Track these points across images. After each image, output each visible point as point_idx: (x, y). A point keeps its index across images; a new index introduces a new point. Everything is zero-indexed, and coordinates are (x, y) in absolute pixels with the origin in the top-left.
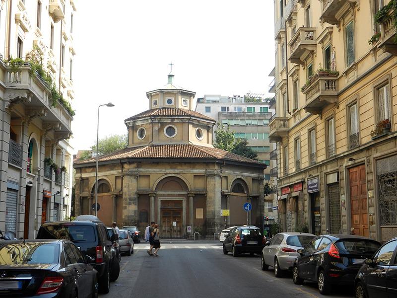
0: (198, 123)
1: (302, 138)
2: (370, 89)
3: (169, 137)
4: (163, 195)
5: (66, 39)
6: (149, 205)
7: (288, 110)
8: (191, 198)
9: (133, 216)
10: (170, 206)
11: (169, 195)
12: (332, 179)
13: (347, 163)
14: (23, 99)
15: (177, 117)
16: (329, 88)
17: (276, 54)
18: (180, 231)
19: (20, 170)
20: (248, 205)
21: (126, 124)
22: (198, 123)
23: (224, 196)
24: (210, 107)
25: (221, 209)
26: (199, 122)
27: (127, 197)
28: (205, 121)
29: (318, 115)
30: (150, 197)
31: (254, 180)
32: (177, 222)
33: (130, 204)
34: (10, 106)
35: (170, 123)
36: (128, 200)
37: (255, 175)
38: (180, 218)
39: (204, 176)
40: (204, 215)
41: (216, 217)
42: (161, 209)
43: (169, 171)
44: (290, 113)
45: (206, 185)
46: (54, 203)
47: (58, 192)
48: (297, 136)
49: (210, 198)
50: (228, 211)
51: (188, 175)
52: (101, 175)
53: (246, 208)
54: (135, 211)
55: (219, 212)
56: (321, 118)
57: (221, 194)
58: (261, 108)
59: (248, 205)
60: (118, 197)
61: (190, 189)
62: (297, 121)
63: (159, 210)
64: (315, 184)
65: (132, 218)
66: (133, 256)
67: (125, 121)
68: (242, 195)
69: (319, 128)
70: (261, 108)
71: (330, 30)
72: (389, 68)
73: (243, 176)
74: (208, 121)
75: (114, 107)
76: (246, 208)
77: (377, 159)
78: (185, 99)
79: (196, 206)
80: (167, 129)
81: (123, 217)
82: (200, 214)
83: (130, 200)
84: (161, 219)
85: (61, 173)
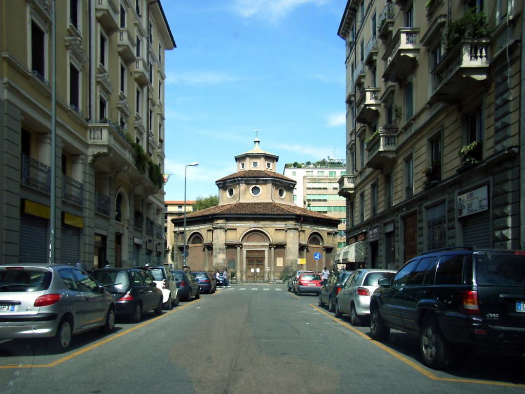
0: (280, 184)
1: (366, 193)
2: (424, 141)
3: (254, 195)
4: (249, 246)
5: (154, 105)
6: (236, 254)
7: (355, 169)
8: (273, 249)
9: (222, 264)
10: (255, 255)
11: (253, 246)
12: (390, 229)
13: (404, 212)
14: (105, 154)
15: (261, 179)
16: (388, 144)
17: (347, 117)
18: (263, 277)
19: (108, 219)
20: (318, 255)
21: (217, 184)
22: (280, 184)
23: (302, 248)
24: (295, 172)
25: (299, 258)
26: (281, 182)
27: (217, 247)
28: (287, 181)
29: (379, 171)
30: (236, 248)
31: (329, 234)
32: (260, 269)
33: (219, 253)
34: (93, 161)
35: (255, 184)
36: (218, 250)
37: (330, 230)
38: (263, 265)
39: (284, 230)
40: (284, 264)
41: (294, 265)
42: (246, 257)
43: (253, 225)
44: (357, 171)
45: (286, 237)
46: (146, 249)
47: (150, 241)
48: (362, 191)
49: (289, 249)
50: (305, 259)
51: (269, 228)
52: (195, 228)
53: (316, 257)
54: (224, 260)
55: (297, 261)
56: (382, 173)
57: (299, 246)
58: (341, 172)
59: (318, 255)
60: (209, 247)
61: (271, 241)
62: (363, 178)
63: (245, 259)
64: (374, 234)
65: (221, 265)
66: (176, 287)
67: (216, 182)
68: (319, 246)
69: (380, 183)
70: (341, 172)
71: (393, 88)
72: (442, 119)
73: (319, 230)
74: (289, 182)
75: (198, 166)
76: (316, 257)
77: (427, 208)
78: (269, 162)
79: (276, 256)
80: (253, 188)
81: (214, 264)
82: (280, 262)
83: (219, 250)
84: (246, 266)
85: (448, 316)
